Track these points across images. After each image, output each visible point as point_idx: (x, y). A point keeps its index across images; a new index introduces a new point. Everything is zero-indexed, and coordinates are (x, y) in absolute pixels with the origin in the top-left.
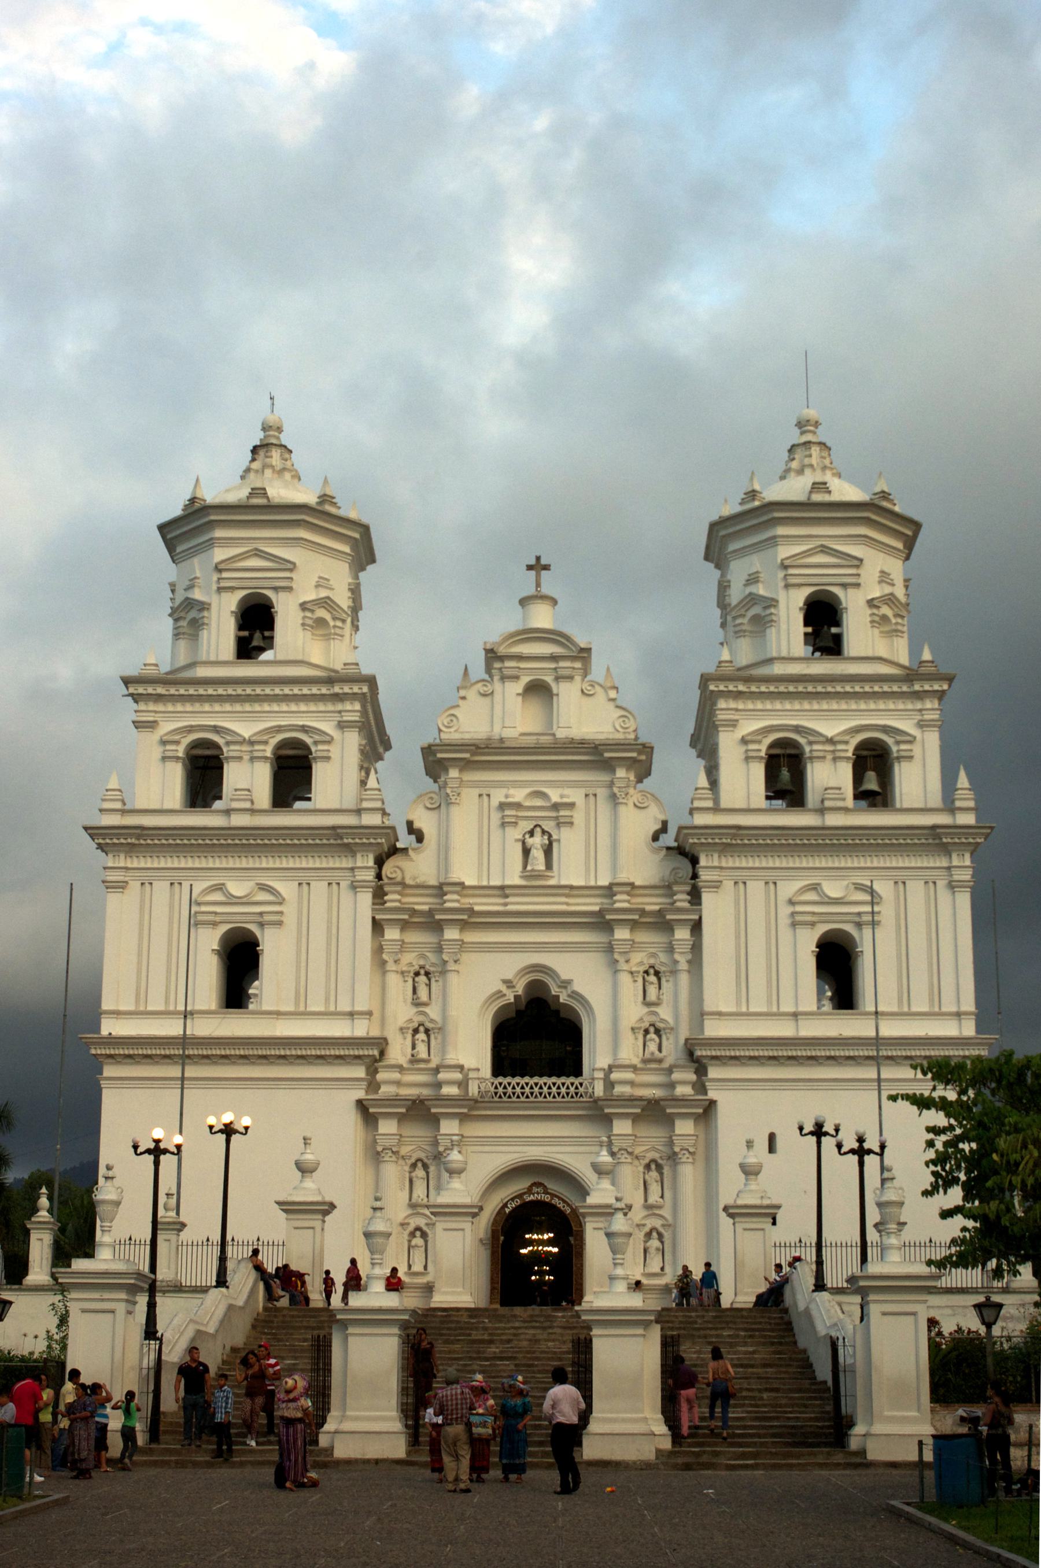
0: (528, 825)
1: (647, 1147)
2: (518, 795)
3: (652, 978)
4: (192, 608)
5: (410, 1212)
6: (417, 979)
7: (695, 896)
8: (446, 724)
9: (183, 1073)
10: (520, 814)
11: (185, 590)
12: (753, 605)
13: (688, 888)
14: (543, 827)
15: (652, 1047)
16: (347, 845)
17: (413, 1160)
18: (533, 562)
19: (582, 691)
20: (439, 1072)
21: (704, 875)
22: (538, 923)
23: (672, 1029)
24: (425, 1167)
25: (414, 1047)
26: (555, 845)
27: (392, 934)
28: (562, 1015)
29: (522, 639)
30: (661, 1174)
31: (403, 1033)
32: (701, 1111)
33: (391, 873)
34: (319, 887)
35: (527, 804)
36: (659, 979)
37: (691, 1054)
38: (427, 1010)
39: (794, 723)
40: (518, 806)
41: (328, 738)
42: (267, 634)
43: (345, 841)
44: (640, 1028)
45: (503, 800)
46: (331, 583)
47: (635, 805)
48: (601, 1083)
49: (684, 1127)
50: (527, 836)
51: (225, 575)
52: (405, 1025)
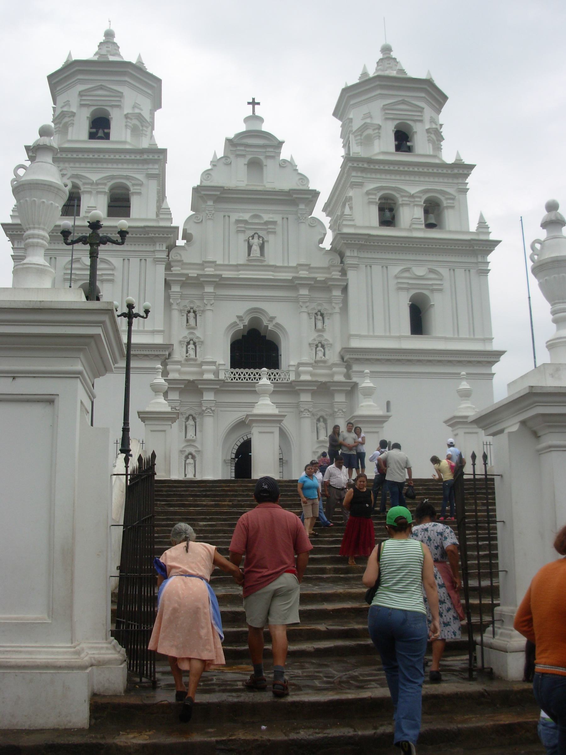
0: (251, 233)
1: (319, 409)
2: (246, 216)
3: (320, 317)
4: (65, 117)
5: (185, 444)
6: (189, 315)
7: (344, 272)
8: (205, 178)
9: (71, 272)
10: (247, 227)
11: (61, 108)
12: (366, 129)
13: (340, 269)
14: (259, 234)
15: (320, 354)
16: (151, 238)
17: (187, 415)
18: (251, 101)
19: (280, 165)
20: (202, 366)
21: (348, 261)
22: (257, 285)
23: (331, 345)
24: (194, 419)
25: (187, 352)
26: (266, 244)
27: (176, 288)
28: (267, 338)
29: (247, 136)
30: (326, 424)
31: (181, 344)
32: (349, 389)
33: (175, 257)
34: (134, 262)
35: (250, 221)
36: (323, 318)
37: (342, 358)
38: (195, 331)
39: (394, 186)
40: (245, 222)
41: (140, 182)
42: (106, 131)
43: (150, 235)
44: (313, 344)
45: (237, 218)
46: (141, 107)
47: (309, 225)
48: (294, 373)
49: (340, 398)
50: (250, 238)
51: (84, 98)
52: (182, 340)
